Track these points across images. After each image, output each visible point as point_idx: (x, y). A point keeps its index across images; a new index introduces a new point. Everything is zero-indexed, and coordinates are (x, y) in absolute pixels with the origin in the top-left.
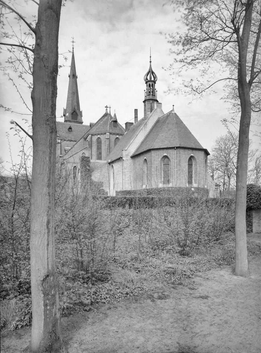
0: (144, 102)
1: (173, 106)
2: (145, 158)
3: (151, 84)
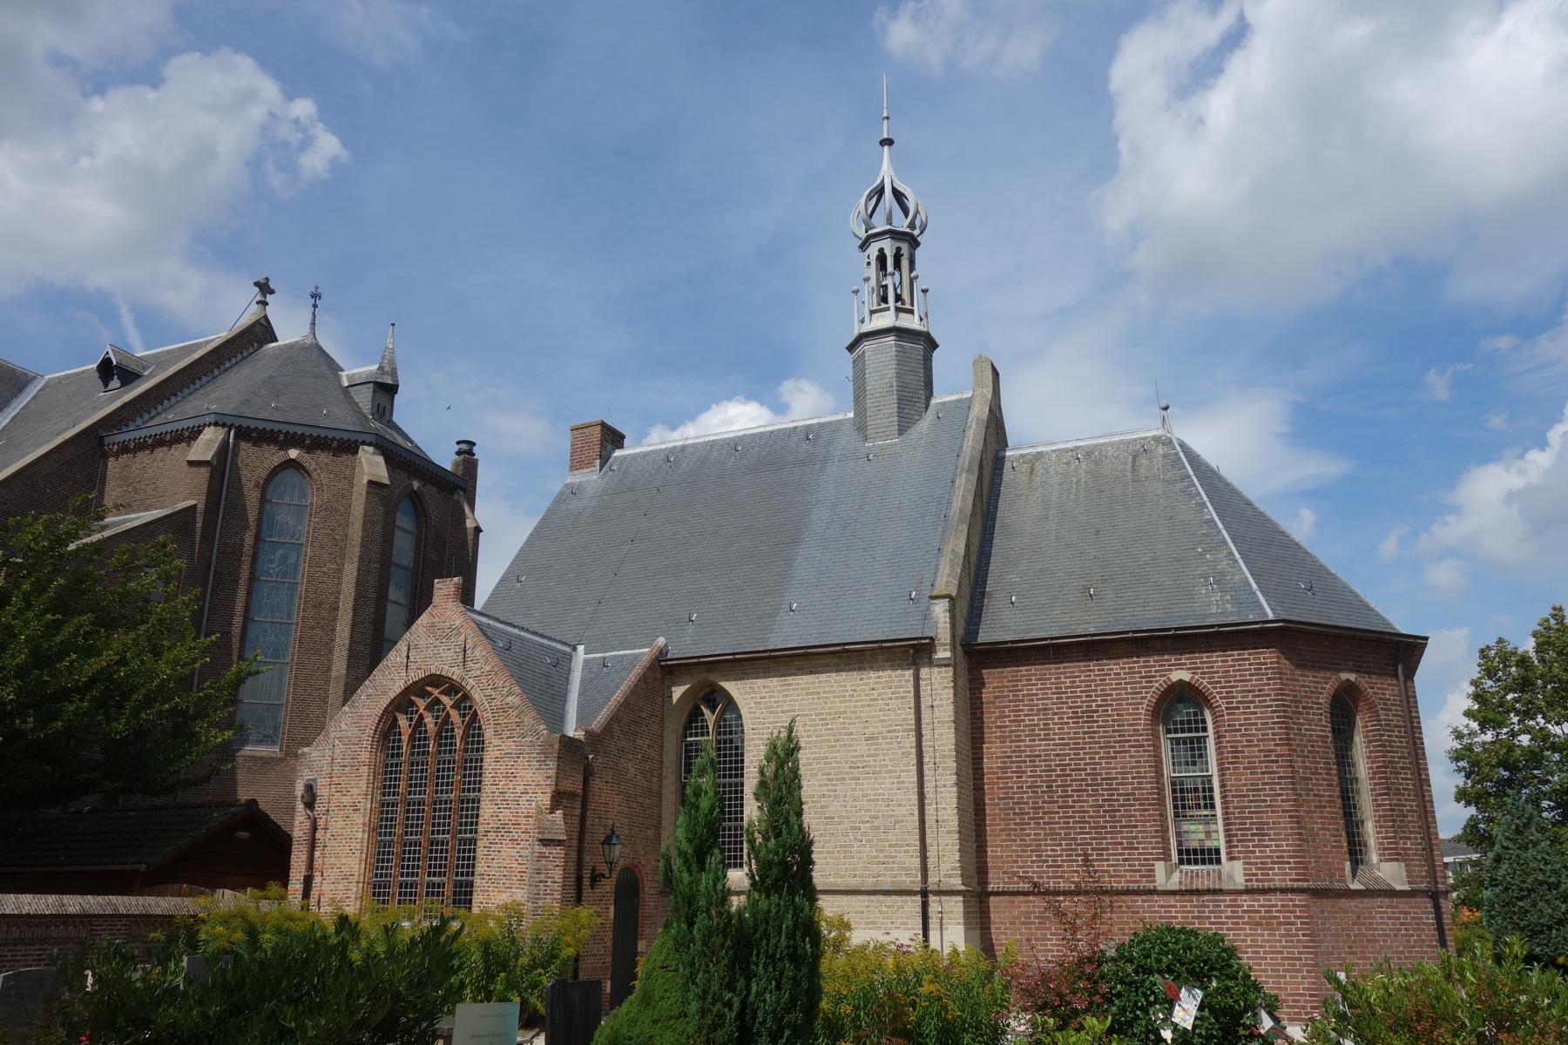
0: (851, 348)
1: (1166, 408)
2: (1176, 676)
3: (889, 253)
